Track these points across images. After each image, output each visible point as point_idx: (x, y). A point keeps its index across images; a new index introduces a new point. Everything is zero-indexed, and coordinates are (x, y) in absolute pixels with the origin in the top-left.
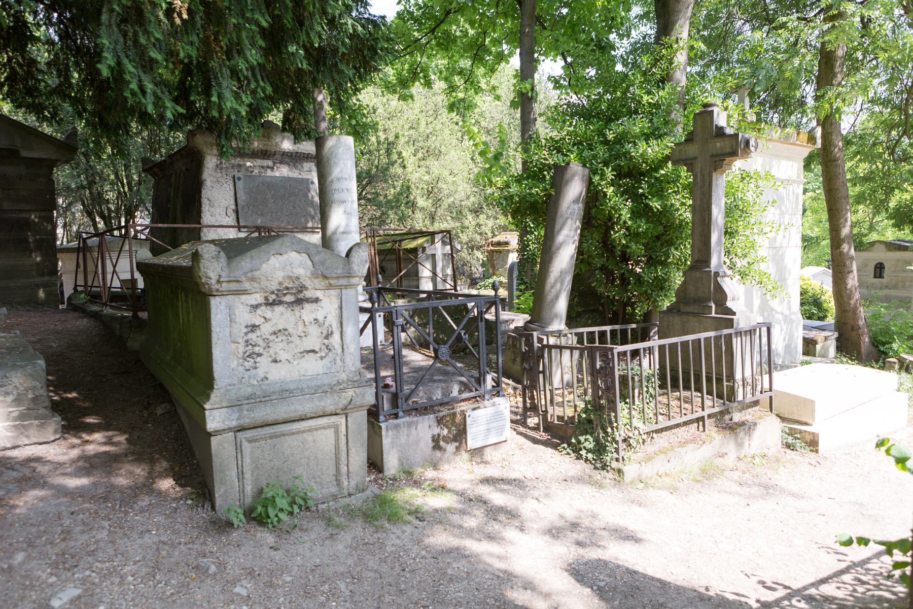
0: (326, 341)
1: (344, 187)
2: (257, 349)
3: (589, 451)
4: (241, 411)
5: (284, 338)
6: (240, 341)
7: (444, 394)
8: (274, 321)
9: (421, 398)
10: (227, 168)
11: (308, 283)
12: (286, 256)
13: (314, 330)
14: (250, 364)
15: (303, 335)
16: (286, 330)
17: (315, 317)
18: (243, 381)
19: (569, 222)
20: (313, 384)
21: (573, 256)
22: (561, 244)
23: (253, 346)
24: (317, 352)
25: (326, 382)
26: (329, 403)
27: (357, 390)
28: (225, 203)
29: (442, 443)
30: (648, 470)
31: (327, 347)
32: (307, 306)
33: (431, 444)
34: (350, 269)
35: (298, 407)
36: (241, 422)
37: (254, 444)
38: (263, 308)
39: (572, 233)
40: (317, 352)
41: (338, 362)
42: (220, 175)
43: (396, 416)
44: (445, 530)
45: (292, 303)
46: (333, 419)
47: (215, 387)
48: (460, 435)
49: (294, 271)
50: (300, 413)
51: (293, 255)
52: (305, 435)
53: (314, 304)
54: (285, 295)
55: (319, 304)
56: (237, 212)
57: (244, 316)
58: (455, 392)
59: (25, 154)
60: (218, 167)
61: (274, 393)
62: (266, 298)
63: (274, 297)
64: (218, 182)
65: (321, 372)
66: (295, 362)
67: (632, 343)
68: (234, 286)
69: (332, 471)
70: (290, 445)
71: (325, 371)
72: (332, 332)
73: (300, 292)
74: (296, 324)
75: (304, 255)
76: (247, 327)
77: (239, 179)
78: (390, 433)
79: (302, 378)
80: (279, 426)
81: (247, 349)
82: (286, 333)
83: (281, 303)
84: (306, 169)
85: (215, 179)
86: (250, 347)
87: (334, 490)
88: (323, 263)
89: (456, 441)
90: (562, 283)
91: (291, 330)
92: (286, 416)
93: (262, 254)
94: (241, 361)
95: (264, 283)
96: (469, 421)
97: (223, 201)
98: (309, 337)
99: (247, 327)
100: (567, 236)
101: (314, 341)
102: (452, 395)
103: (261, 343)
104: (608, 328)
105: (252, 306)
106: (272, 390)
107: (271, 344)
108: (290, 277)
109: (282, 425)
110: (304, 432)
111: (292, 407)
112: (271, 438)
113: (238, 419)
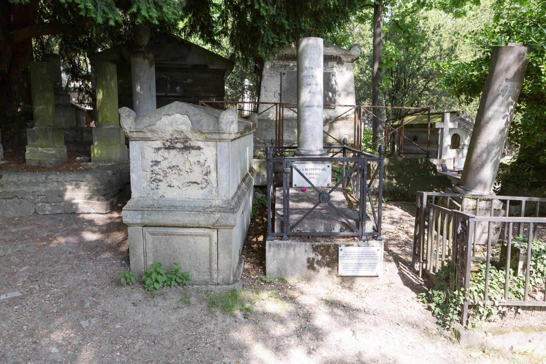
0: (205, 177)
1: (310, 74)
2: (158, 177)
3: (438, 305)
4: (143, 214)
5: (176, 171)
6: (148, 170)
7: (326, 229)
8: (170, 160)
9: (306, 228)
10: (278, 67)
11: (190, 136)
12: (173, 116)
13: (197, 169)
14: (154, 186)
15: (189, 171)
16: (178, 166)
17: (198, 160)
18: (149, 196)
19: (500, 99)
20: (192, 205)
21: (502, 131)
22: (490, 119)
23: (156, 174)
24: (199, 184)
25: (202, 205)
26: (202, 219)
27: (223, 214)
28: (274, 89)
29: (316, 265)
30: (495, 342)
31: (206, 181)
32: (193, 152)
33: (307, 264)
34: (219, 127)
35: (180, 219)
36: (144, 221)
37: (154, 236)
38: (163, 150)
39: (502, 109)
40: (199, 184)
41: (214, 192)
42: (273, 72)
43: (282, 238)
44: (253, 331)
45: (180, 149)
46: (207, 231)
47: (132, 197)
48: (332, 261)
49: (179, 127)
50: (182, 223)
51: (178, 116)
52: (188, 237)
53: (198, 151)
54: (176, 143)
55: (201, 151)
56: (280, 95)
57: (151, 155)
58: (337, 228)
59: (211, 67)
60: (272, 67)
61: (165, 206)
62: (164, 144)
63: (169, 144)
64: (271, 76)
65: (200, 197)
66: (184, 189)
67: (540, 216)
68: (140, 135)
69: (207, 265)
70: (178, 241)
71: (203, 197)
72: (210, 172)
73: (187, 141)
74: (184, 163)
75: (186, 116)
76: (152, 162)
77: (284, 74)
78: (272, 249)
79: (187, 200)
80: (170, 228)
81: (152, 176)
82: (178, 168)
83: (174, 148)
84: (330, 66)
85: (269, 75)
86: (154, 175)
87: (207, 278)
88: (198, 122)
89: (329, 266)
90: (489, 153)
91: (181, 167)
92: (172, 223)
93: (157, 114)
94: (149, 183)
95: (160, 134)
96: (341, 254)
97: (273, 88)
98: (193, 173)
99: (152, 162)
100: (496, 111)
101: (197, 176)
102: (333, 231)
103: (161, 173)
104: (524, 199)
105: (156, 149)
106: (165, 204)
107: (168, 175)
108: (177, 131)
109: (172, 228)
110: (187, 235)
111: (176, 218)
112: (165, 235)
113: (141, 219)
